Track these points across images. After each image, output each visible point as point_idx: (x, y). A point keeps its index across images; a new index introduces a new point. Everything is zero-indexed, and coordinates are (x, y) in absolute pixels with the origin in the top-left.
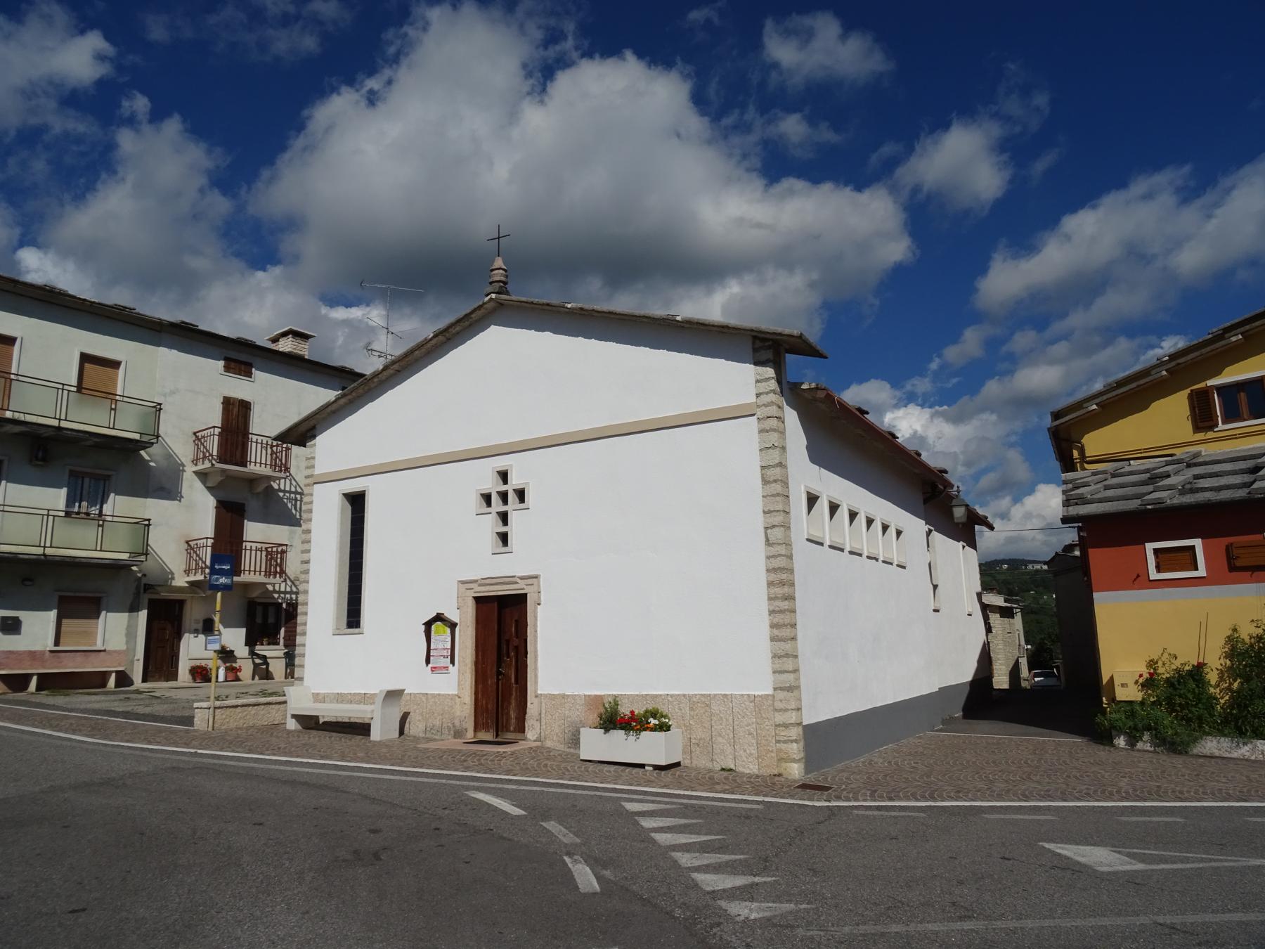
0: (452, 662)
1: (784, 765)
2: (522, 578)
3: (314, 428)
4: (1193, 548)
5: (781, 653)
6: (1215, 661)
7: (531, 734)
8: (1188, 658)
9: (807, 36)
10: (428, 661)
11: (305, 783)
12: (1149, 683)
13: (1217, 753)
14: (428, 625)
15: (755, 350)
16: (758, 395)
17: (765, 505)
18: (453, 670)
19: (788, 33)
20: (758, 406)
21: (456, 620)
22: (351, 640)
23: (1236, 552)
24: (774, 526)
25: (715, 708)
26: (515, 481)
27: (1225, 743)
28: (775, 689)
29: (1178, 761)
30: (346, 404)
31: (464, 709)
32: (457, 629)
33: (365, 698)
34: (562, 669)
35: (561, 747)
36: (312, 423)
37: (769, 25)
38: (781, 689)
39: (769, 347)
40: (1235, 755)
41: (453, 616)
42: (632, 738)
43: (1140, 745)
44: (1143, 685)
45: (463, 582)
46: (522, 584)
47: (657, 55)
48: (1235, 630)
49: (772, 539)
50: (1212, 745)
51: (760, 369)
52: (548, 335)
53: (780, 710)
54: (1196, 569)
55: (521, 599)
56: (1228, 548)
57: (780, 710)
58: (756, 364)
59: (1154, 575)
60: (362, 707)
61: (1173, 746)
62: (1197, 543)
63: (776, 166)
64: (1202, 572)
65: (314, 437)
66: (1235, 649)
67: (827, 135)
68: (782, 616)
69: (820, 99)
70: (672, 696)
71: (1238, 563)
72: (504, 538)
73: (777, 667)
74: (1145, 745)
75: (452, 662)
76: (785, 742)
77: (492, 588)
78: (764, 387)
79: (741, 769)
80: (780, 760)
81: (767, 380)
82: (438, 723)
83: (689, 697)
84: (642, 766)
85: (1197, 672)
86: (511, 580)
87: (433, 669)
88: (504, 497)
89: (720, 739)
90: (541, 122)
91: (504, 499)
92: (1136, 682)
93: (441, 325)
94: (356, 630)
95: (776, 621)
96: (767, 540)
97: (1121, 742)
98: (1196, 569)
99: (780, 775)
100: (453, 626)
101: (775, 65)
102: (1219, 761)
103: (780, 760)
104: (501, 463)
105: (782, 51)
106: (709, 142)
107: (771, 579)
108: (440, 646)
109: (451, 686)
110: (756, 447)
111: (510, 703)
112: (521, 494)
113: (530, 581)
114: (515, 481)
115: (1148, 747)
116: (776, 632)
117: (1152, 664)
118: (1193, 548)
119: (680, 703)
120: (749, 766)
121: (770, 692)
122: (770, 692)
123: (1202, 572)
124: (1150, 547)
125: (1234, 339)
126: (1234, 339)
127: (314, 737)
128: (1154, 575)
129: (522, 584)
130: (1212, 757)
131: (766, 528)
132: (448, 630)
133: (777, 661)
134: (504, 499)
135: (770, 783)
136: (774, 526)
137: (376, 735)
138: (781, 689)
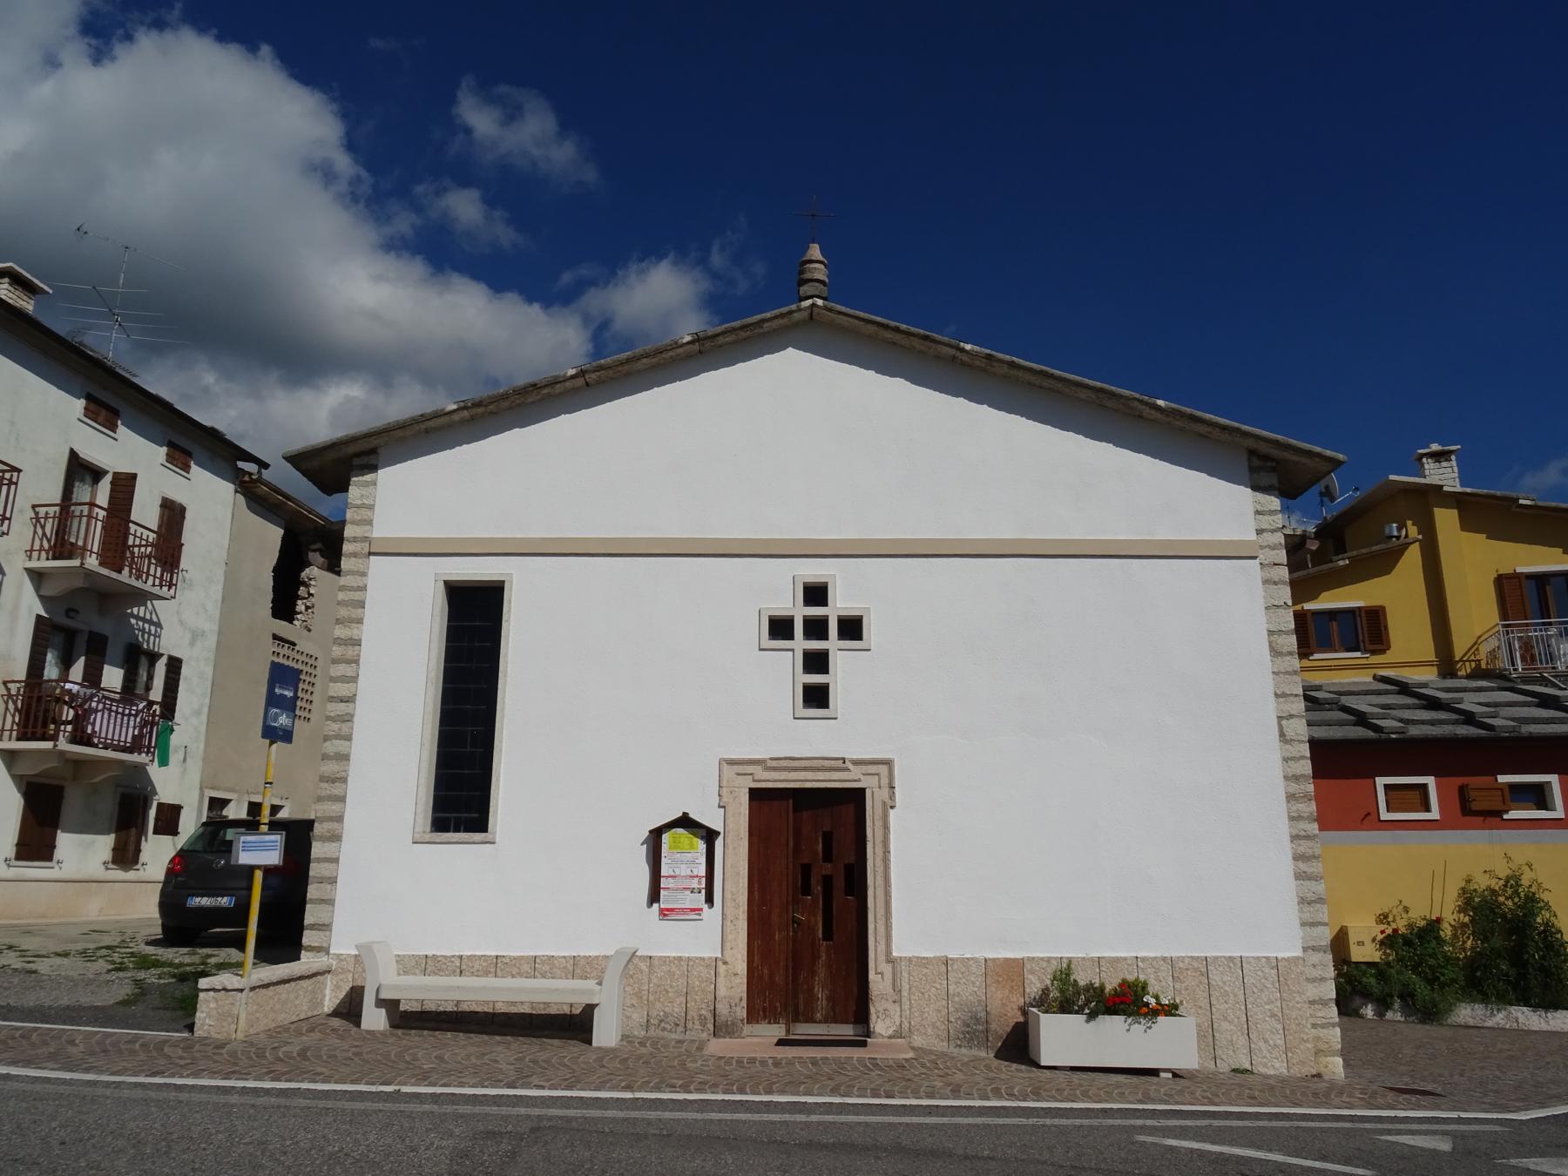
0: (710, 900)
1: (1323, 1060)
2: (856, 763)
3: (373, 451)
4: (1425, 786)
5: (1310, 896)
6: (1450, 915)
7: (881, 1025)
8: (1420, 913)
9: (512, 114)
10: (654, 897)
11: (811, 1145)
12: (1388, 942)
13: (1471, 1022)
14: (657, 834)
15: (1252, 470)
16: (1259, 532)
17: (1276, 685)
18: (712, 916)
19: (490, 100)
20: (1262, 547)
21: (716, 825)
22: (459, 852)
23: (1473, 794)
24: (1291, 716)
25: (1215, 977)
26: (840, 604)
27: (1479, 1009)
28: (1305, 949)
29: (1421, 1031)
30: (462, 422)
31: (733, 986)
32: (719, 843)
33: (578, 967)
34: (937, 914)
35: (941, 1046)
36: (374, 442)
37: (467, 82)
38: (1314, 949)
39: (1273, 470)
40: (1489, 1024)
41: (713, 820)
42: (1138, 1029)
43: (1389, 1015)
44: (1382, 943)
45: (731, 762)
46: (856, 772)
47: (304, 67)
48: (1468, 881)
49: (1290, 733)
50: (1467, 1013)
51: (1260, 496)
52: (899, 382)
53: (1313, 980)
54: (1428, 810)
55: (854, 799)
56: (1462, 790)
57: (1313, 980)
58: (1255, 488)
59: (1385, 816)
60: (491, 981)
61: (1429, 1014)
62: (1430, 781)
63: (440, 252)
64: (1435, 814)
65: (373, 468)
66: (1468, 901)
67: (506, 235)
68: (1310, 843)
69: (510, 188)
70: (1144, 959)
71: (1475, 806)
72: (816, 697)
73: (1307, 917)
74: (1394, 1015)
75: (710, 900)
76: (1323, 1026)
77: (793, 775)
78: (1266, 522)
79: (1262, 1070)
80: (1318, 1052)
81: (1272, 512)
82: (677, 1009)
83: (1171, 962)
84: (1154, 1072)
85: (1434, 925)
86: (841, 764)
87: (664, 913)
88: (816, 628)
89: (1225, 1025)
90: (98, 91)
91: (816, 633)
92: (1374, 940)
93: (712, 331)
94: (478, 836)
95: (1301, 850)
96: (1282, 734)
97: (1369, 1011)
98: (1428, 810)
99: (1319, 1075)
100: (710, 836)
101: (468, 131)
102: (1475, 1032)
103: (1318, 1052)
104: (814, 570)
105: (480, 119)
106: (354, 198)
107: (1291, 790)
108: (684, 870)
109: (709, 940)
110: (1260, 604)
111: (813, 973)
112: (852, 628)
113: (872, 769)
114: (840, 604)
115: (1398, 1017)
116: (1303, 866)
117: (1383, 918)
118: (1425, 786)
119: (1157, 970)
120: (1273, 1065)
121: (1298, 953)
122: (1298, 953)
123: (1435, 814)
124: (1381, 781)
125: (1341, 563)
126: (1341, 563)
127: (422, 1043)
128: (1385, 816)
129: (856, 772)
130: (1468, 1027)
131: (1280, 718)
132: (701, 846)
133: (1306, 908)
134: (816, 633)
135: (1313, 1087)
136: (1291, 716)
137: (606, 1033)
138: (1314, 949)
